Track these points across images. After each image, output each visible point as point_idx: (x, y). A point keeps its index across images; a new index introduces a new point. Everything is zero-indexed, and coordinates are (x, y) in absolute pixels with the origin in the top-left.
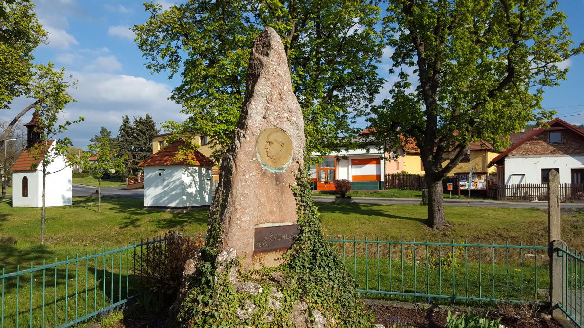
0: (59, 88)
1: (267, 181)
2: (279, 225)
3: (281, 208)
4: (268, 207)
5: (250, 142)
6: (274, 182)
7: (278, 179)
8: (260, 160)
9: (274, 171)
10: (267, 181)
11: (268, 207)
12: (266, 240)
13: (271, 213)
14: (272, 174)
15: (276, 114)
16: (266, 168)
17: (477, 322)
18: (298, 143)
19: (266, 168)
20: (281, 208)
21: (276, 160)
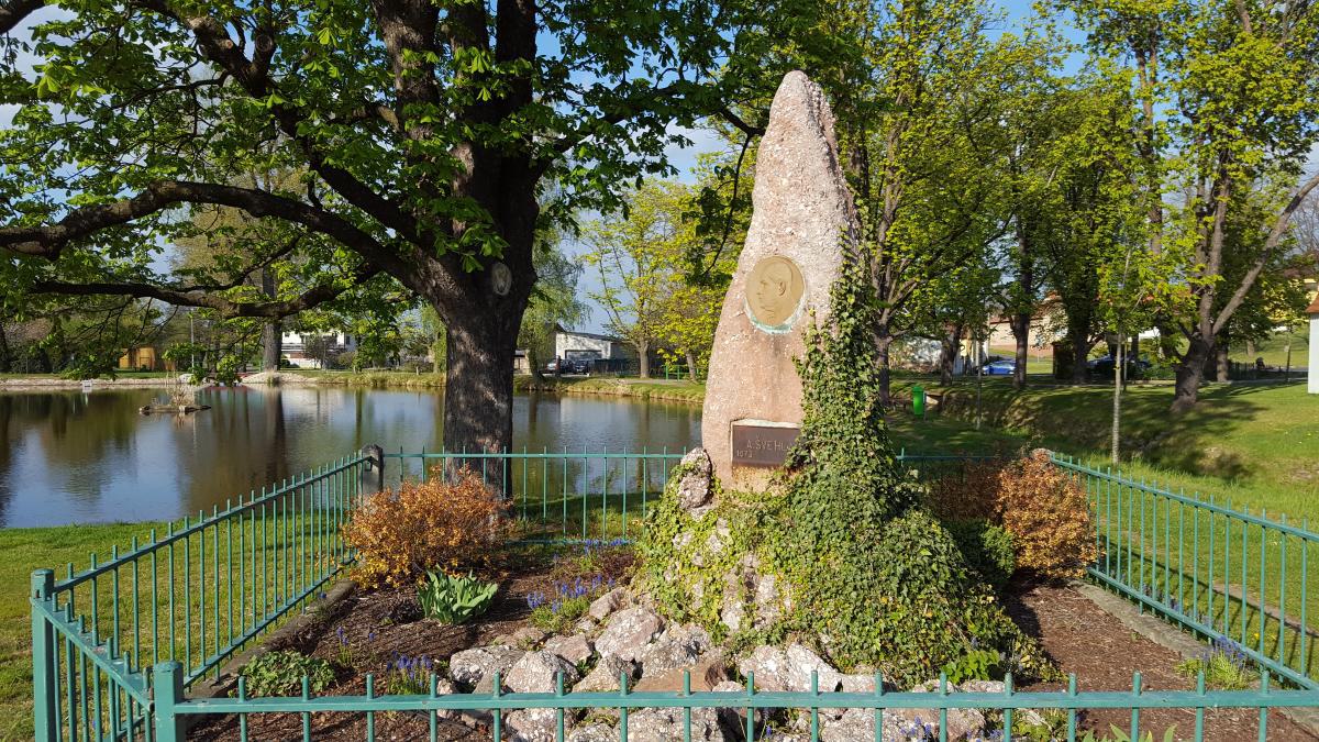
0: (708, 346)
1: (757, 348)
2: (770, 424)
3: (775, 396)
4: (753, 393)
5: (739, 284)
6: (771, 351)
7: (777, 344)
8: (749, 315)
9: (770, 332)
10: (757, 348)
11: (753, 393)
12: (752, 447)
13: (758, 402)
14: (768, 338)
15: (774, 231)
16: (758, 326)
17: (776, 6)
18: (1104, 524)
19: (758, 326)
20: (775, 396)
21: (775, 314)
